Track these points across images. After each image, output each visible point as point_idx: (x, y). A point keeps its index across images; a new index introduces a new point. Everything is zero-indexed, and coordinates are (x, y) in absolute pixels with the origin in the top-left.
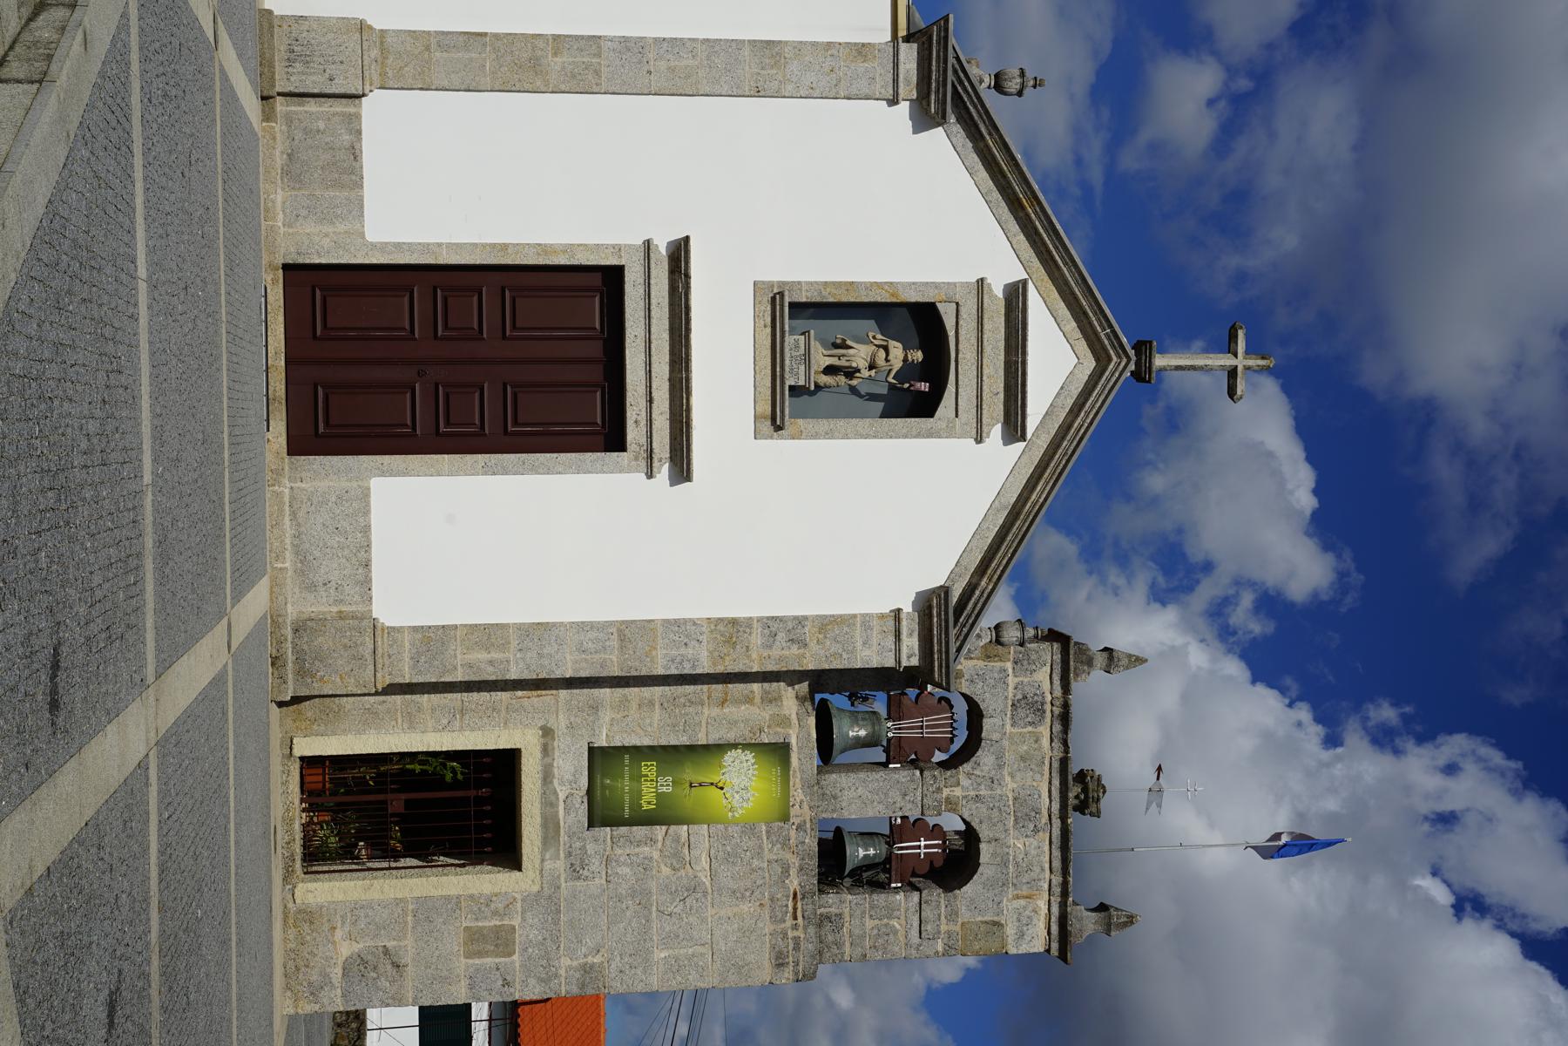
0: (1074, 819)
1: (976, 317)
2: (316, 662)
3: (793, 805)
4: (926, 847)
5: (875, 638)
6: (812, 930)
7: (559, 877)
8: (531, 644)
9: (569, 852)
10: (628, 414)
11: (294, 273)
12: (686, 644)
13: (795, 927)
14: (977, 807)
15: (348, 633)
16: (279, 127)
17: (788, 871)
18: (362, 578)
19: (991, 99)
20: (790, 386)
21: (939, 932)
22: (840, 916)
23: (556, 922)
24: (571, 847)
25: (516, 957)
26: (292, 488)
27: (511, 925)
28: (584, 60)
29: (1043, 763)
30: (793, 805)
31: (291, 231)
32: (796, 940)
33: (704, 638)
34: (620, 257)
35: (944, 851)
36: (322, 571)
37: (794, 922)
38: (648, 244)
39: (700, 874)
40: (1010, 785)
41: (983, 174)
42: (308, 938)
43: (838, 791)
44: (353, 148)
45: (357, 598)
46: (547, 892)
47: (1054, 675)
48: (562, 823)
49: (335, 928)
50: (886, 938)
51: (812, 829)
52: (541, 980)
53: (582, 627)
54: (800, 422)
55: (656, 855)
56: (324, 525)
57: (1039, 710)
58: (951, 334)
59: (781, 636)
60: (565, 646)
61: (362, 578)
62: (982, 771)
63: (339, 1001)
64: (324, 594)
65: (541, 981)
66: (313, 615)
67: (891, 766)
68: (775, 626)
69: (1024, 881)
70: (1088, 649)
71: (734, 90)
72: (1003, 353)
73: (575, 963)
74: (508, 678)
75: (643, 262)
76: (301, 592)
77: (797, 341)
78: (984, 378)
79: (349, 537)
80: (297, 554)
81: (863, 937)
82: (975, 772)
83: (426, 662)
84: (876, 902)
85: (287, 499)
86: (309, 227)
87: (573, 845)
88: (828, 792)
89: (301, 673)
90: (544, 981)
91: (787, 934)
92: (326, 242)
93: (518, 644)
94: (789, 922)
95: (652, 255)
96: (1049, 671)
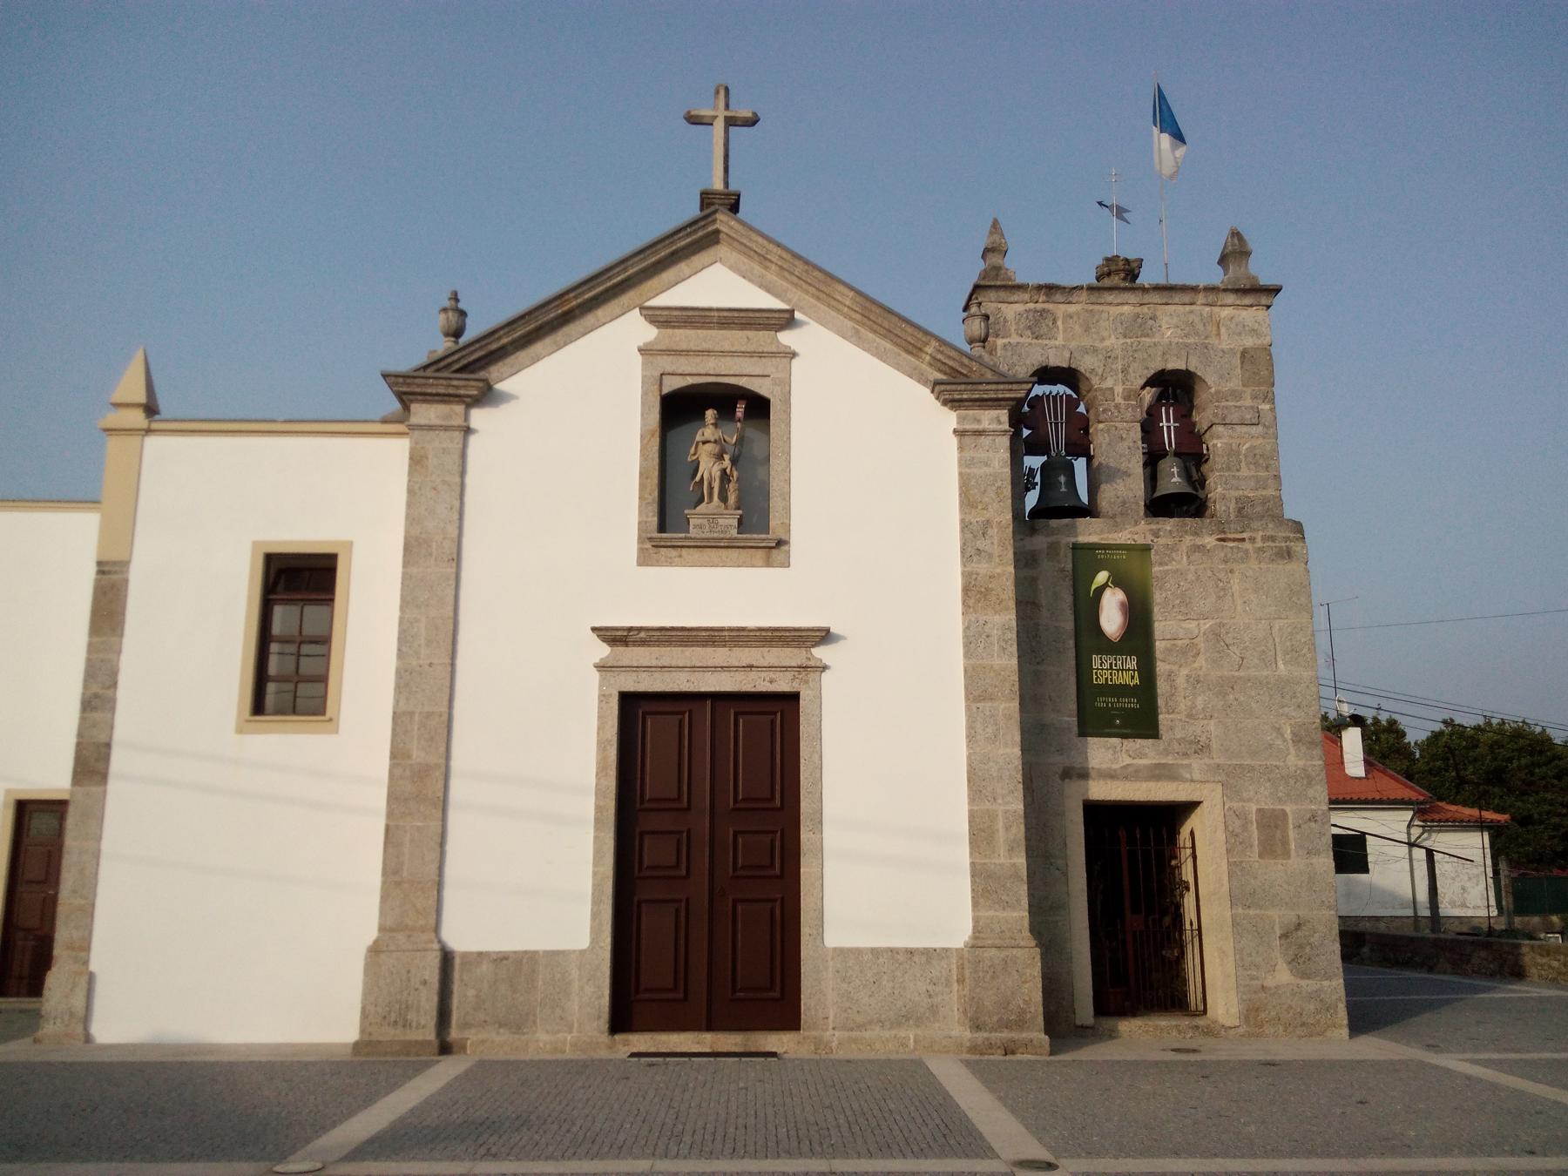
0: (1144, 279)
1: (675, 357)
2: (1010, 1008)
3: (1134, 541)
4: (1168, 420)
5: (981, 455)
6: (1255, 525)
7: (1208, 765)
8: (988, 789)
9: (1183, 755)
10: (764, 689)
11: (622, 1019)
12: (988, 636)
13: (1253, 540)
14: (1134, 372)
15: (981, 974)
16: (472, 1036)
17: (1199, 547)
18: (924, 959)
19: (463, 340)
20: (738, 533)
21: (1252, 407)
22: (1238, 500)
23: (1252, 769)
24: (1178, 753)
25: (1288, 809)
26: (834, 1029)
27: (1256, 813)
28: (416, 728)
29: (1091, 311)
30: (1134, 541)
31: (576, 1025)
32: (1265, 539)
33: (982, 618)
34: (611, 695)
35: (1172, 405)
36: (917, 999)
37: (1247, 540)
38: (601, 667)
39: (1202, 630)
40: (1112, 342)
41: (538, 347)
42: (1272, 1013)
43: (1119, 501)
44: (496, 960)
45: (944, 963)
46: (1223, 778)
47: (1009, 300)
48: (1154, 762)
49: (1263, 986)
50: (1258, 457)
51: (1158, 523)
52: (1310, 784)
53: (971, 737)
54: (772, 523)
55: (1184, 672)
56: (870, 996)
57: (1041, 315)
58: (690, 381)
59: (980, 544)
60: (990, 755)
61: (924, 959)
62: (1099, 367)
63: (1334, 983)
64: (940, 998)
65: (1310, 784)
66: (961, 1010)
67: (1092, 453)
68: (970, 551)
69: (1202, 329)
70: (985, 270)
71: (451, 582)
72: (710, 332)
73: (1292, 751)
74: (1022, 813)
75: (616, 673)
76: (938, 1021)
77: (695, 527)
78: (733, 350)
79: (883, 970)
80: (899, 1024)
81: (1258, 479)
82: (1100, 374)
83: (1008, 895)
84: (1224, 466)
85: (847, 1034)
86: (574, 1006)
87: (1176, 751)
88: (1120, 510)
89: (1021, 1023)
90: (1310, 781)
91: (1259, 548)
92: (589, 989)
93: (989, 801)
94: (1247, 545)
95: (609, 664)
96: (1006, 305)
